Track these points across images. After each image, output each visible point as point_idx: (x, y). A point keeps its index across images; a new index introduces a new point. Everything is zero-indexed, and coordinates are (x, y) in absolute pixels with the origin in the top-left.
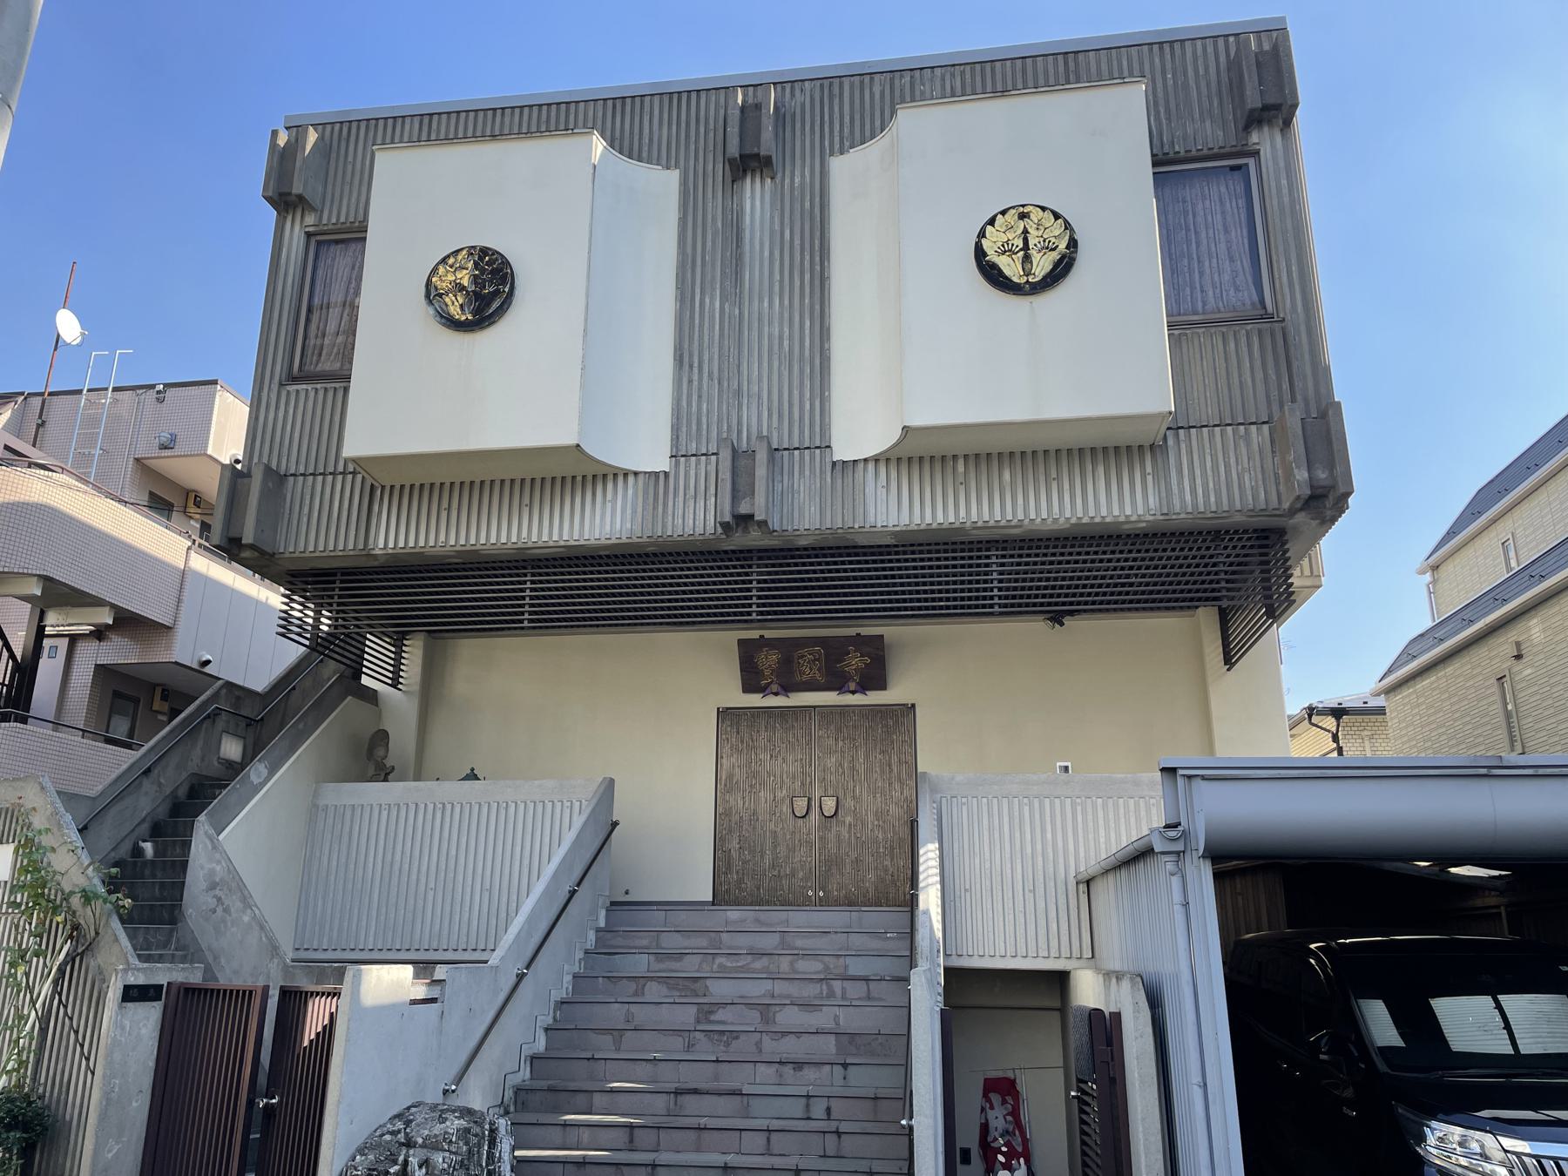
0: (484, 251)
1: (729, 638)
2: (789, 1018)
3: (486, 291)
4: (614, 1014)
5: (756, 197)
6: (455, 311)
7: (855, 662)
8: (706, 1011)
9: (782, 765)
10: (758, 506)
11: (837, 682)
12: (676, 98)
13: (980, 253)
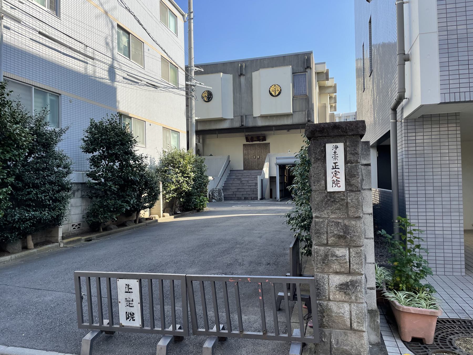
0: (208, 91)
1: (243, 134)
2: (250, 182)
3: (209, 97)
4: (231, 182)
5: (243, 78)
6: (206, 100)
7: (261, 138)
8: (241, 182)
9: (251, 152)
10: (244, 124)
11: (259, 140)
12: (232, 63)
13: (270, 91)
